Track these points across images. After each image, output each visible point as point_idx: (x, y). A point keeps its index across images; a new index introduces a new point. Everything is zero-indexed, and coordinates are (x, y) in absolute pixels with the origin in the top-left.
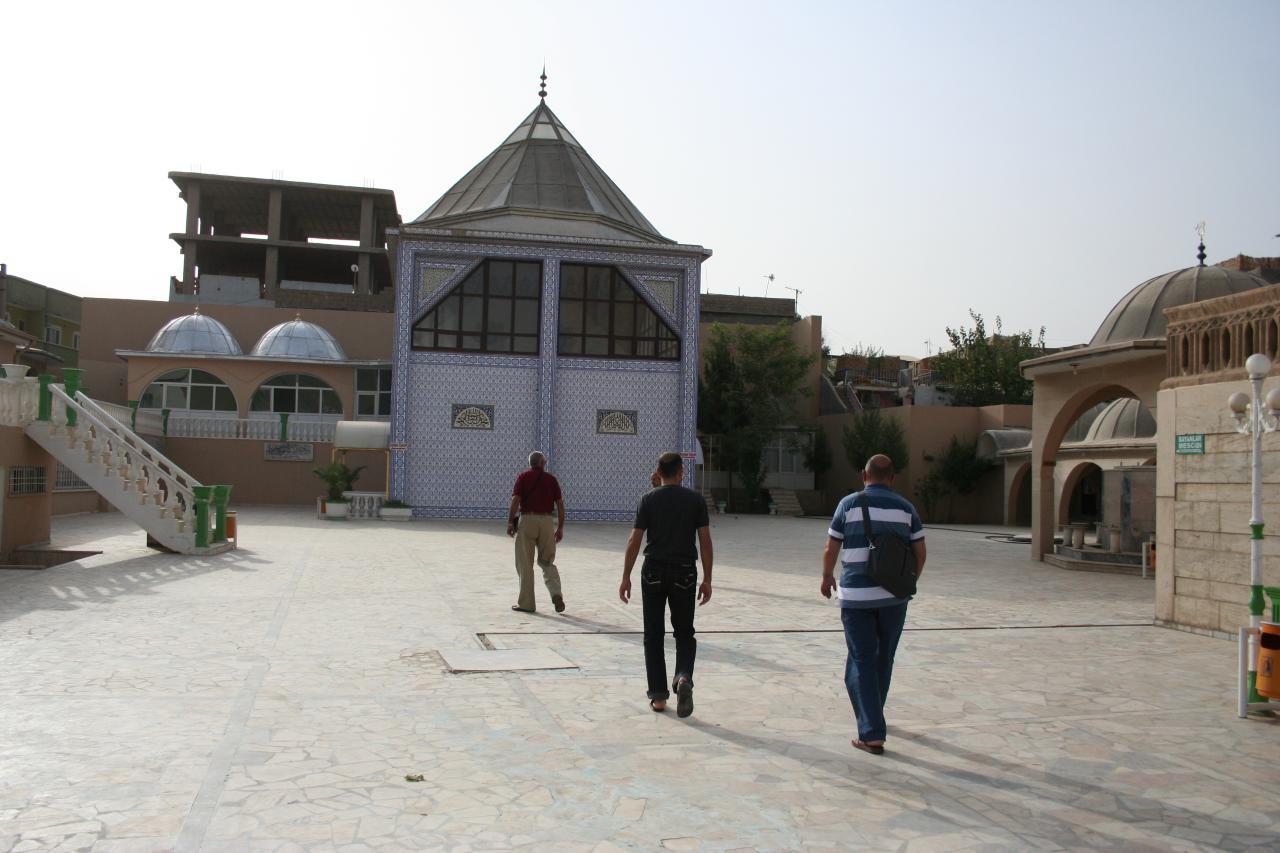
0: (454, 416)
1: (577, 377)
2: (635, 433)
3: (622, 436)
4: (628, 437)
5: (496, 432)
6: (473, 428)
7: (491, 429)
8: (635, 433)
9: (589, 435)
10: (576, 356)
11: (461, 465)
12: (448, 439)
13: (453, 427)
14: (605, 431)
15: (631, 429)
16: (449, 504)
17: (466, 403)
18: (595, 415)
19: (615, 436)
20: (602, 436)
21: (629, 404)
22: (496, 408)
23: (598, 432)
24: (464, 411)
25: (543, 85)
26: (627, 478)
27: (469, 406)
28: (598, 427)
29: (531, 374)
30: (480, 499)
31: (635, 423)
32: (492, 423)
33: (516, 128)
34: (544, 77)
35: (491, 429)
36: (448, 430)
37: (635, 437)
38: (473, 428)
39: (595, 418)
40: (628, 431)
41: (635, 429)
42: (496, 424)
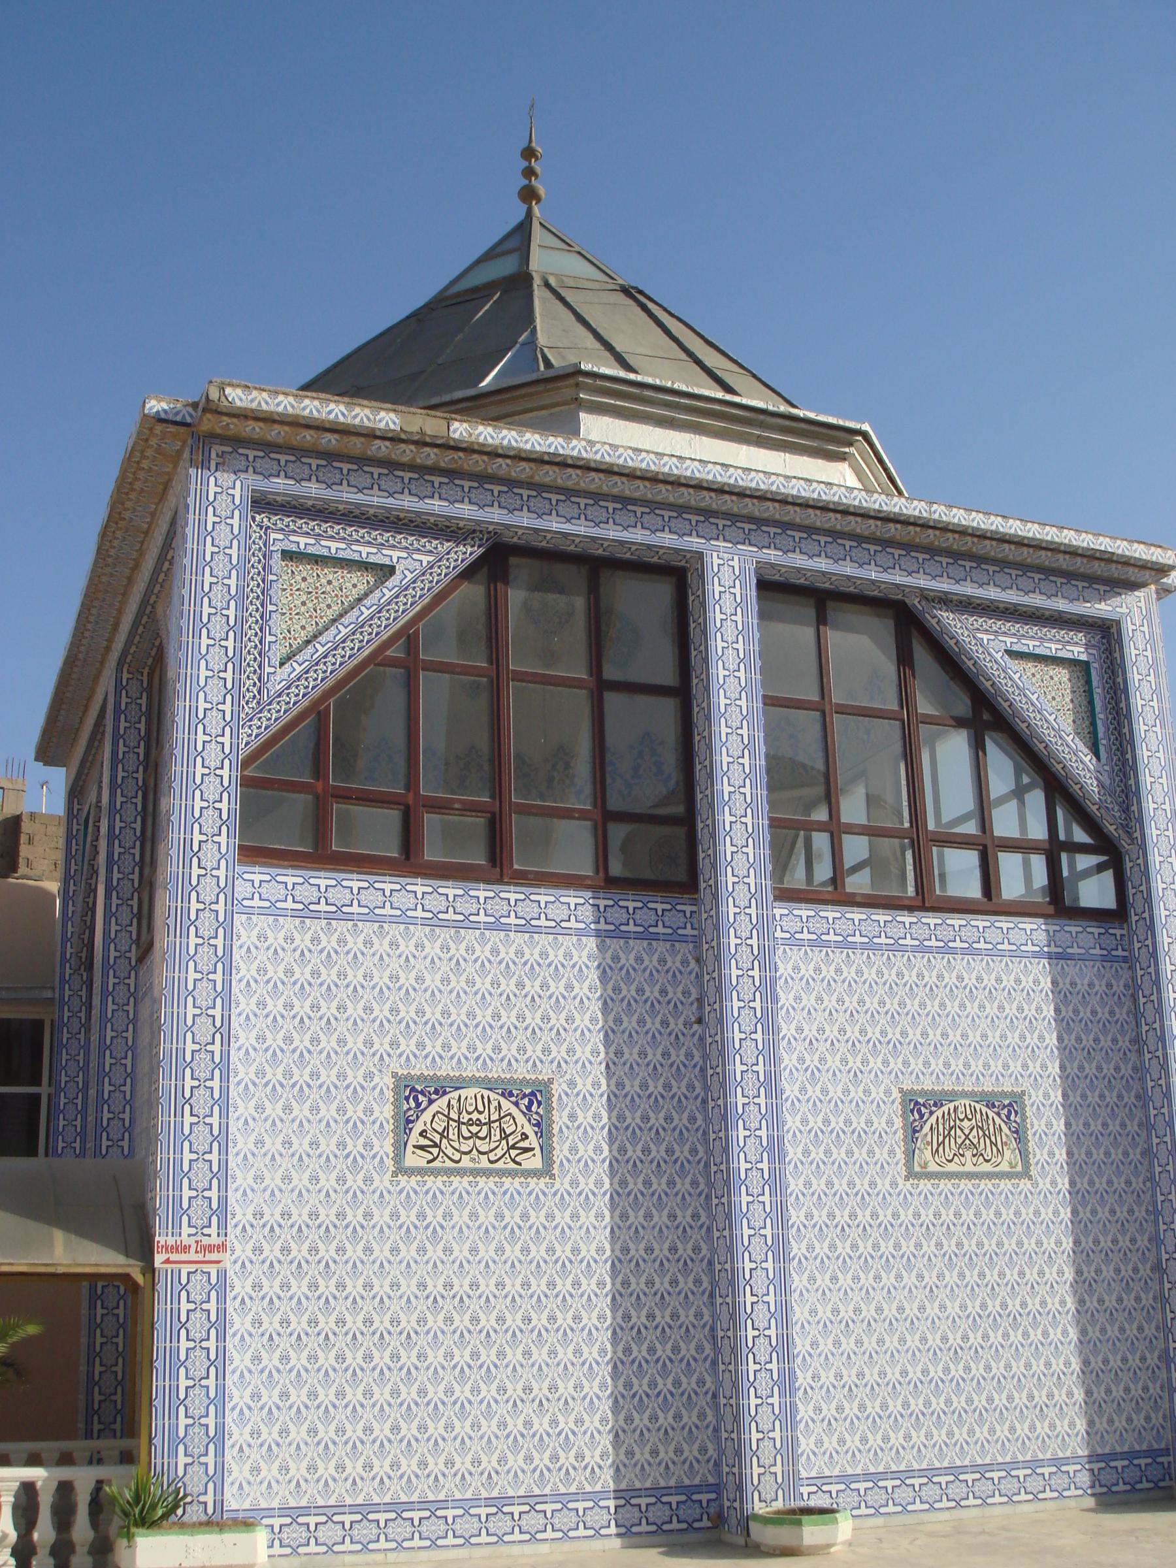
0: (405, 1123)
1: (849, 973)
2: (1026, 1174)
3: (986, 1185)
4: (1005, 1185)
5: (562, 1184)
6: (476, 1172)
7: (546, 1171)
8: (1026, 1174)
9: (883, 1185)
10: (911, 909)
11: (435, 1322)
12: (381, 1217)
13: (401, 1170)
14: (933, 1167)
15: (1009, 1158)
16: (395, 1491)
17: (446, 1070)
18: (894, 1110)
19: (966, 1185)
20: (925, 1185)
21: (510, 1050)
22: (557, 1089)
23: (910, 1174)
24: (442, 1103)
25: (529, 173)
26: (513, 1252)
27: (459, 1084)
28: (910, 1154)
29: (674, 963)
30: (515, 1461)
31: (1019, 1134)
32: (547, 1151)
33: (500, 236)
34: (529, 153)
35: (546, 1171)
36: (383, 1181)
37: (1025, 1185)
38: (476, 1172)
39: (898, 1123)
40: (1004, 1167)
41: (1024, 1154)
42: (561, 1151)
